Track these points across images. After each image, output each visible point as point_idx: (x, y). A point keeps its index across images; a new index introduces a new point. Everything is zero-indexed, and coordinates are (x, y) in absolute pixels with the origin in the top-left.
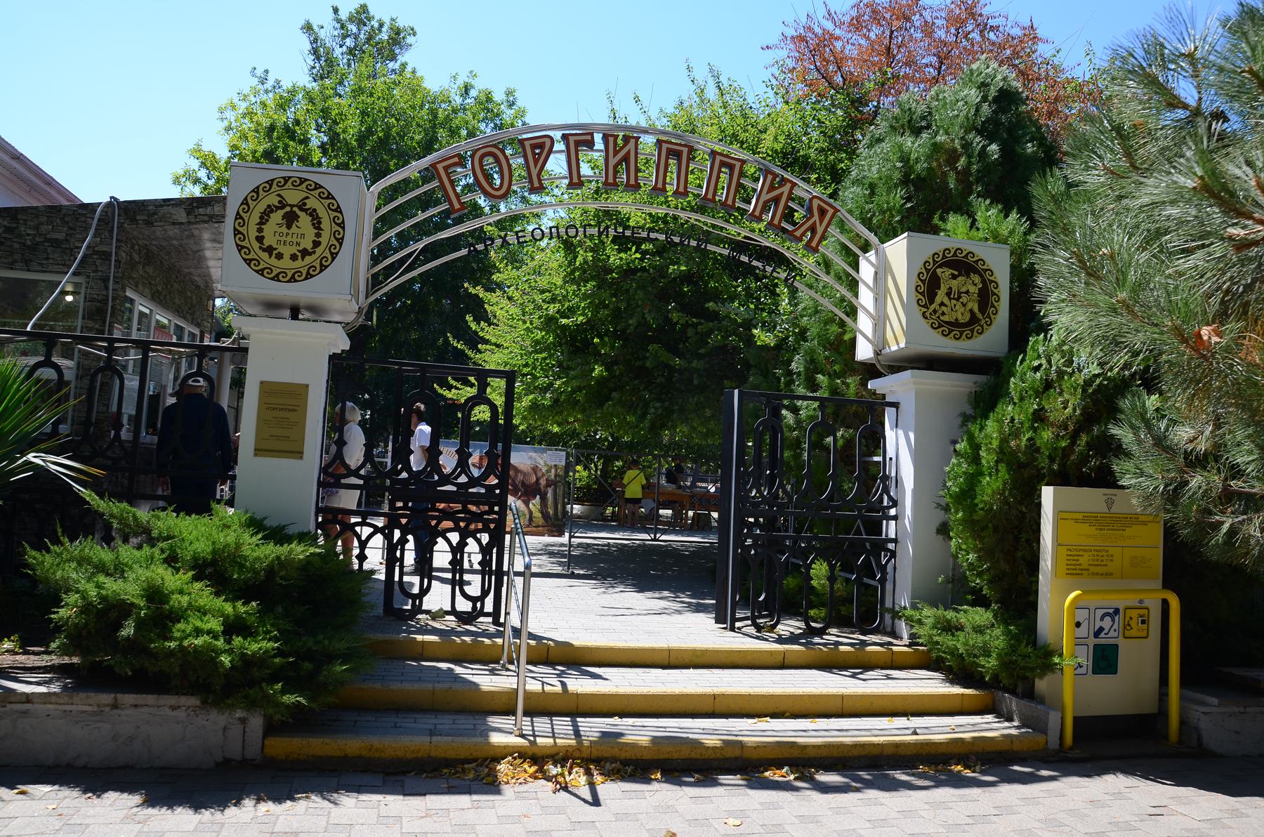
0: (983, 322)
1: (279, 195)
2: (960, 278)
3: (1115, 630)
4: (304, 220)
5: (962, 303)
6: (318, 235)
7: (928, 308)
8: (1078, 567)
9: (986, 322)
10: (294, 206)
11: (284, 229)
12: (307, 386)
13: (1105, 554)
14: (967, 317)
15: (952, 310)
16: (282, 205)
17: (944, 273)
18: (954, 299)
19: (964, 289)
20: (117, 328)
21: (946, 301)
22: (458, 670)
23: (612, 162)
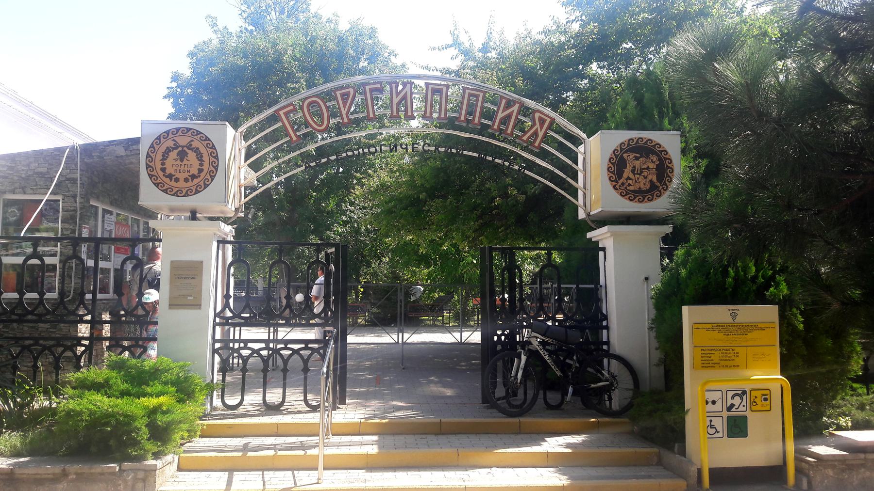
0: (661, 188)
1: (174, 140)
2: (641, 159)
3: (744, 406)
4: (191, 155)
5: (644, 176)
6: (201, 165)
7: (617, 182)
8: (710, 362)
9: (663, 188)
10: (184, 146)
11: (179, 162)
12: (202, 262)
13: (731, 351)
14: (648, 186)
15: (636, 182)
16: (176, 146)
17: (629, 157)
18: (637, 174)
19: (645, 166)
20: (85, 228)
21: (631, 176)
22: (15, 460)
23: (396, 101)
